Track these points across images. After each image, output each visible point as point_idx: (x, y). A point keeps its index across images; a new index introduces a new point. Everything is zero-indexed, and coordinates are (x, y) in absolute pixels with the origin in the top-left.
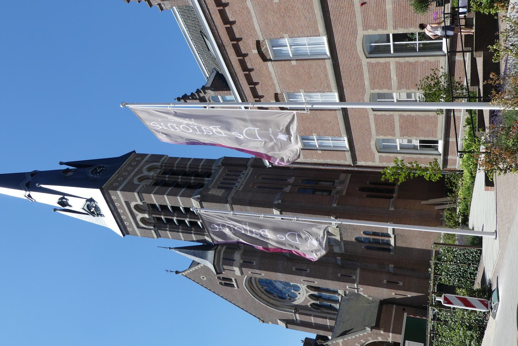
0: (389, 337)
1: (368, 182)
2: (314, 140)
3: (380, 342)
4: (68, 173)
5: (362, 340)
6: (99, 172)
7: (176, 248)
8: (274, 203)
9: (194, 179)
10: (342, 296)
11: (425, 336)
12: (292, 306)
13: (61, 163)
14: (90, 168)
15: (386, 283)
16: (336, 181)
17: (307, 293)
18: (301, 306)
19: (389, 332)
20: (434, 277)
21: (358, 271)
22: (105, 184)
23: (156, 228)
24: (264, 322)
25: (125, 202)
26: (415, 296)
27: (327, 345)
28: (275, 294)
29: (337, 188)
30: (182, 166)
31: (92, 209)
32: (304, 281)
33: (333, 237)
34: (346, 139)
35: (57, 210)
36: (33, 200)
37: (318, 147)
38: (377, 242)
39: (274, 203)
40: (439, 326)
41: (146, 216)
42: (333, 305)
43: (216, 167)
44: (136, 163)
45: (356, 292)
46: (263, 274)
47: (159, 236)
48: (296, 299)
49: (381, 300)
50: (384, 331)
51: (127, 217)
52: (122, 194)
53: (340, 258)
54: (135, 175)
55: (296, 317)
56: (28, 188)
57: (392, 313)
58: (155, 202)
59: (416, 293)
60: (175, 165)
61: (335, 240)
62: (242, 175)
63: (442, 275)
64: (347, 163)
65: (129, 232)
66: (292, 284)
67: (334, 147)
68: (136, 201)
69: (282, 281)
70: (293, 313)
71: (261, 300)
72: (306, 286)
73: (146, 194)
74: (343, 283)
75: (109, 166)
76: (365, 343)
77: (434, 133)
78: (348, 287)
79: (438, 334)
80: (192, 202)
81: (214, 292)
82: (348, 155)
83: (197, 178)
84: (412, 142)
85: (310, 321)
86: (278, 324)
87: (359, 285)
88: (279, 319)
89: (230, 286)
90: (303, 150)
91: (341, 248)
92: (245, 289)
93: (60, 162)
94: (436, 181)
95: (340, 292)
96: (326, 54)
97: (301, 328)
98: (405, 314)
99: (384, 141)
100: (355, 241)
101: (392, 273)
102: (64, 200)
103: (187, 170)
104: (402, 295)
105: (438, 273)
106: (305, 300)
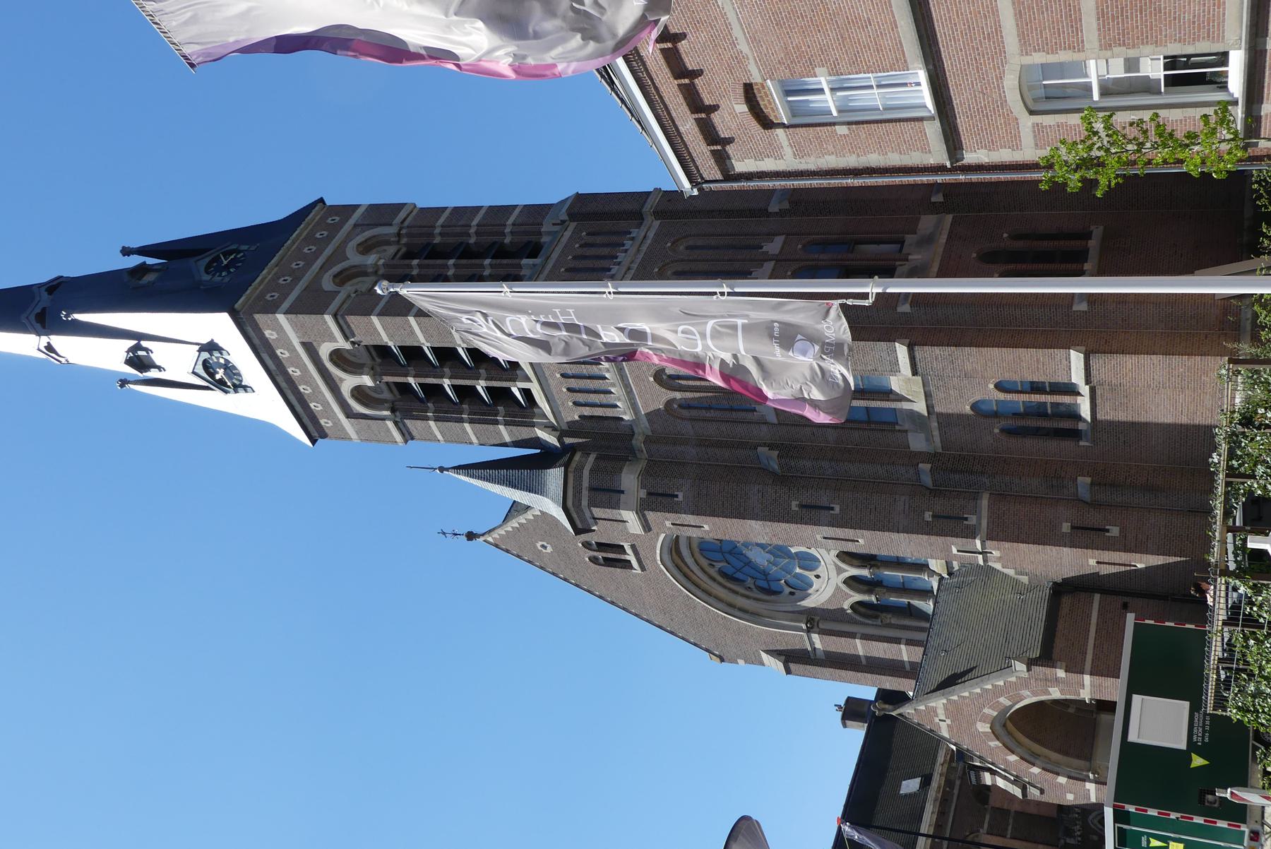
0: (1083, 686)
1: (1005, 235)
2: (821, 91)
3: (1056, 702)
4: (143, 277)
5: (1002, 700)
6: (227, 267)
7: (458, 468)
9: (491, 265)
10: (942, 578)
11: (1200, 679)
13: (126, 252)
14: (200, 257)
16: (910, 239)
17: (838, 574)
18: (823, 610)
20: (1228, 484)
21: (984, 502)
22: (241, 296)
23: (398, 414)
24: (722, 660)
25: (304, 344)
26: (1157, 566)
27: (900, 715)
28: (750, 582)
29: (910, 257)
30: (458, 230)
31: (218, 373)
32: (825, 538)
33: (905, 406)
34: (922, 76)
35: (129, 382)
36: (63, 360)
37: (835, 113)
38: (1039, 411)
40: (1252, 642)
41: (367, 381)
42: (916, 602)
43: (554, 224)
44: (326, 233)
45: (981, 562)
46: (706, 527)
47: (408, 436)
49: (1055, 583)
50: (1066, 672)
51: (315, 388)
52: (295, 326)
53: (929, 466)
54: (323, 268)
55: (812, 643)
56: (44, 327)
57: (1089, 616)
58: (386, 339)
59: (1161, 557)
60: (437, 231)
61: (913, 415)
62: (628, 243)
63: (1253, 477)
64: (932, 160)
65: (327, 431)
66: (793, 550)
67: (887, 109)
68: (333, 339)
69: (764, 542)
70: (802, 630)
71: (711, 600)
72: (834, 553)
73: (358, 318)
74: (940, 540)
75: (253, 248)
76: (1011, 707)
77: (1212, 26)
78: (954, 551)
79: (1244, 671)
81: (577, 585)
82: (933, 130)
83: (498, 261)
84: (1141, 68)
85: (899, 658)
86: (763, 665)
87: (988, 543)
88: (764, 651)
89: (620, 565)
90: (791, 130)
91: (929, 439)
93: (123, 247)
94: (1223, 176)
95: (936, 565)
96: (926, 107)
97: (828, 671)
98: (1131, 618)
99: (1047, 70)
100: (972, 413)
101: (1087, 503)
102: (141, 353)
103: (472, 240)
104: (1120, 565)
105: (1242, 469)
106: (833, 595)
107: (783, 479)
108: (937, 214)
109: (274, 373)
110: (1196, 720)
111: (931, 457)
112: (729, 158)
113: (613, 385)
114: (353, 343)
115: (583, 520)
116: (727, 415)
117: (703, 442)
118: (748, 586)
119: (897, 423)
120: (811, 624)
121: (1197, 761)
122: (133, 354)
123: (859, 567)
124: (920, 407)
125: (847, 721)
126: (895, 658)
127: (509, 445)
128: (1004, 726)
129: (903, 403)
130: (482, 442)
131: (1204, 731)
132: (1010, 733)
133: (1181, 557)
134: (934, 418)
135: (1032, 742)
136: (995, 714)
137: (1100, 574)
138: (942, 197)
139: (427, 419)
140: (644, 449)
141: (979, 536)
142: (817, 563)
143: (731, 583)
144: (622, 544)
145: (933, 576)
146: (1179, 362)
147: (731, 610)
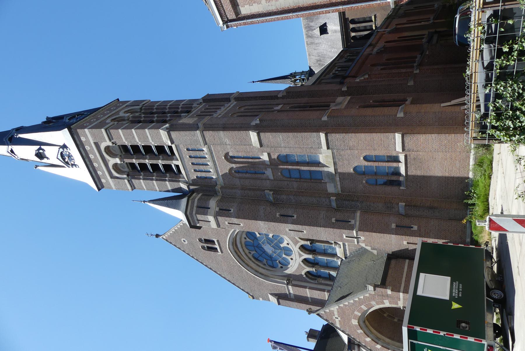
5: (363, 307)
8: (251, 124)
10: (342, 260)
12: (285, 276)
15: (395, 227)
18: (294, 275)
19: (399, 291)
21: (358, 214)
23: (130, 177)
24: (253, 298)
33: (326, 169)
39: (251, 124)
45: (356, 243)
47: (133, 187)
48: (289, 266)
49: (388, 254)
50: (392, 291)
51: (99, 164)
55: (289, 291)
57: (403, 268)
61: (329, 173)
70: (285, 284)
71: (249, 268)
80: (161, 136)
81: (197, 260)
86: (270, 301)
87: (359, 232)
88: (270, 294)
91: (335, 187)
92: (229, 253)
93: (47, 117)
101: (403, 215)
106: (298, 268)
107: (275, 204)
108: (344, 96)
109: (85, 157)
110: (454, 286)
111: (337, 195)
112: (238, 6)
113: (209, 161)
114: (113, 143)
115: (194, 221)
116: (253, 176)
117: (243, 188)
118: (264, 263)
119: (323, 180)
120: (289, 281)
121: (455, 306)
122: (38, 151)
123: (308, 254)
124: (332, 170)
125: (309, 338)
126: (323, 299)
127: (170, 191)
128: (364, 322)
129: (324, 168)
130: (160, 190)
131: (459, 291)
132: (367, 326)
133: (445, 240)
134: (338, 175)
135: (377, 333)
136: (360, 314)
137: (409, 249)
138: (346, 88)
139: (140, 179)
140: (220, 191)
141: (355, 229)
142: (292, 252)
143: (258, 262)
144: (214, 240)
145: (338, 259)
146: (444, 138)
147: (256, 273)
